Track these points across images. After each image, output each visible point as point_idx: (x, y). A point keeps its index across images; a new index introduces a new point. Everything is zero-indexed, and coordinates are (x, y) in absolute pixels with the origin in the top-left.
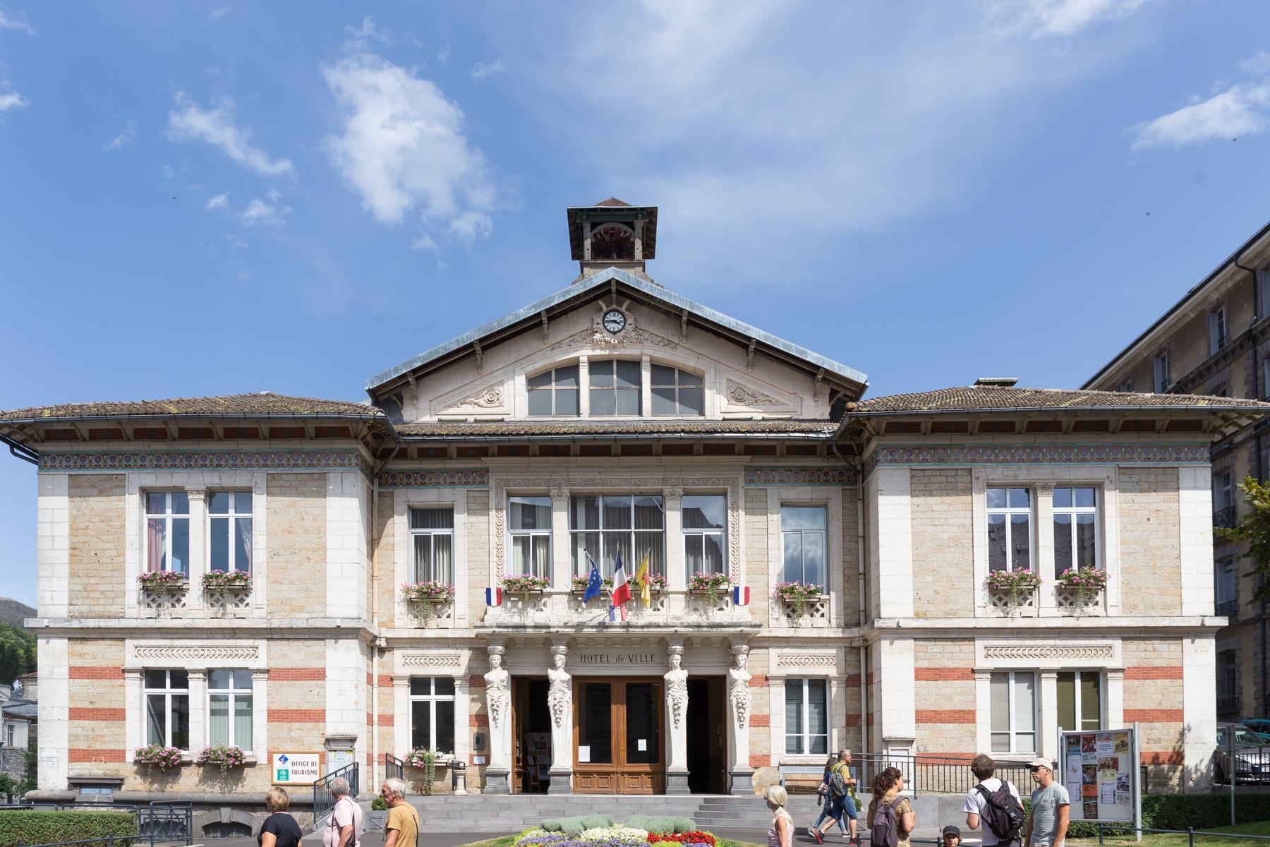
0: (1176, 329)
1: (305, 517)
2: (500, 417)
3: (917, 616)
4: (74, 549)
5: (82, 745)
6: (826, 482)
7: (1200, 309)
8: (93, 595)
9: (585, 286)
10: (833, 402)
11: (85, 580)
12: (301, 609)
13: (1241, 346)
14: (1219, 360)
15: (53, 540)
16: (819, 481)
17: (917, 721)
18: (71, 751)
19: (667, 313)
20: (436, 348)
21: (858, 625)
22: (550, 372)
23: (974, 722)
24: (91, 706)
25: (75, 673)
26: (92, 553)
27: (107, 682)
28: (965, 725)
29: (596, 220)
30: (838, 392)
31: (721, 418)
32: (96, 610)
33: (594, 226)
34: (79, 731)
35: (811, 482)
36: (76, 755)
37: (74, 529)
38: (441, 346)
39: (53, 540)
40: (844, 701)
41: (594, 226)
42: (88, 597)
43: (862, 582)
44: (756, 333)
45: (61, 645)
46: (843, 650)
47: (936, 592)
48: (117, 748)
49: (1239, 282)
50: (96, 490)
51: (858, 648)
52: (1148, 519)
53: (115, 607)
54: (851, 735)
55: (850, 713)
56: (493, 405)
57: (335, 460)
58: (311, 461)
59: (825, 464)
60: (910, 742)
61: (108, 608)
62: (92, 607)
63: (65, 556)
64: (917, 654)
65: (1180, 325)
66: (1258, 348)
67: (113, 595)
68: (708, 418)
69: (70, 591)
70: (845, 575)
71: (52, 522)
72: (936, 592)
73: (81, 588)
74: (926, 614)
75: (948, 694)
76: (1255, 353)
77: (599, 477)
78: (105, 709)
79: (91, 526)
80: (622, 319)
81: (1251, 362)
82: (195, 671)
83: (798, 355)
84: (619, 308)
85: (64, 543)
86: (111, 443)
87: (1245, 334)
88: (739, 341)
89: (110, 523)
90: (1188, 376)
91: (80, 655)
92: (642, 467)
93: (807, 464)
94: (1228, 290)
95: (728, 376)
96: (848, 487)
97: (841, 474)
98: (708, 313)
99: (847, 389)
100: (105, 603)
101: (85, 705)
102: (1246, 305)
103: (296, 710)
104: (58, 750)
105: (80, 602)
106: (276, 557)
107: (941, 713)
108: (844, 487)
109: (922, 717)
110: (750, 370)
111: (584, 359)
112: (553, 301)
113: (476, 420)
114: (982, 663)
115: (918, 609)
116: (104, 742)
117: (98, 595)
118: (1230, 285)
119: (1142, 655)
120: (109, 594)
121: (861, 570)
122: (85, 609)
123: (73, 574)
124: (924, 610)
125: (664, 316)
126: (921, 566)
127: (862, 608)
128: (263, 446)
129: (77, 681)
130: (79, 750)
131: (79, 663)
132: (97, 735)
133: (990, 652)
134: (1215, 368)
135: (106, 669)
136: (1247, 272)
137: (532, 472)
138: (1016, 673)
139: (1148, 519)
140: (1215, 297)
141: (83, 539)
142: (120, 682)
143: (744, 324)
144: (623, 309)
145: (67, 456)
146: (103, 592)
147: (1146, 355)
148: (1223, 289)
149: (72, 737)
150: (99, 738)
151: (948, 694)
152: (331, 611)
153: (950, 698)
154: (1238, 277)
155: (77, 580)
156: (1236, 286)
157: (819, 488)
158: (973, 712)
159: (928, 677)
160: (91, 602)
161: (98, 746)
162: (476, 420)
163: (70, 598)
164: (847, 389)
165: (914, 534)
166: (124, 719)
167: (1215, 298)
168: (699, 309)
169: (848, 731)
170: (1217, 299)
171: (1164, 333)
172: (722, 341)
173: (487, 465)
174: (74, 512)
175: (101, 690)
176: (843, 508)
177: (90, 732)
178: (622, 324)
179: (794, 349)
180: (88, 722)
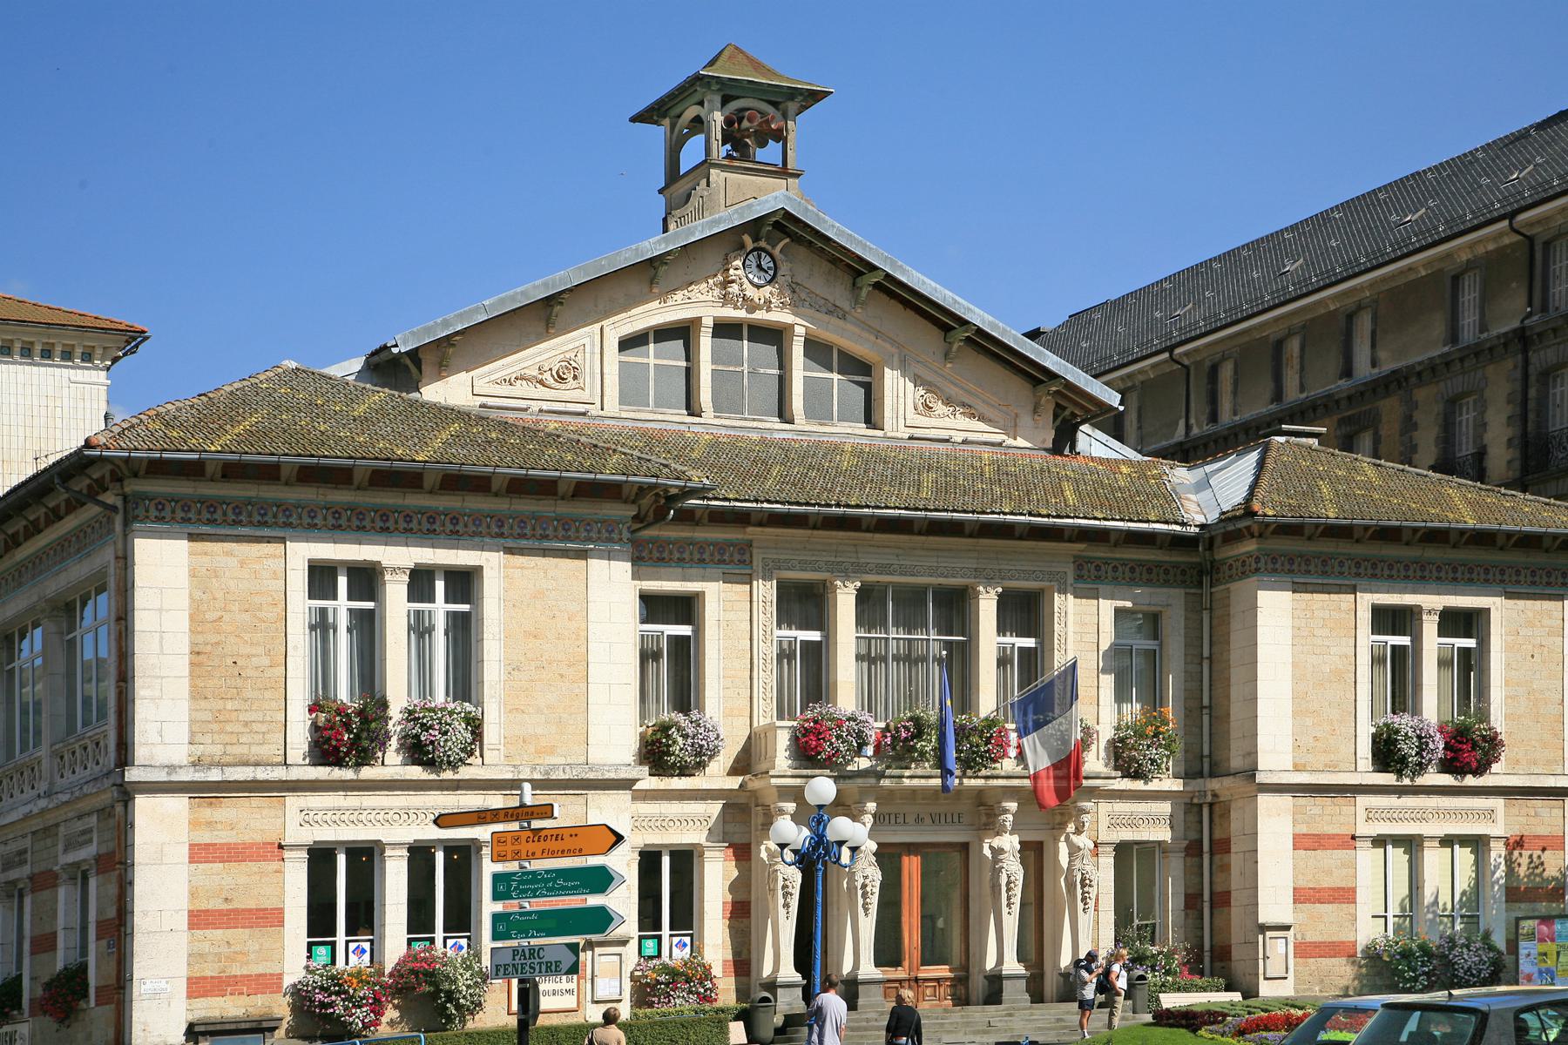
0: (1393, 284)
1: (558, 614)
2: (580, 408)
3: (1297, 768)
4: (198, 653)
5: (210, 970)
6: (1166, 583)
7: (1437, 266)
8: (229, 728)
9: (742, 217)
10: (1058, 422)
11: (220, 704)
12: (551, 750)
13: (1505, 345)
14: (1468, 355)
15: (162, 638)
16: (1158, 580)
17: (1295, 902)
18: (191, 981)
19: (834, 261)
20: (511, 292)
21: (1200, 775)
22: (647, 334)
23: (1354, 902)
24: (225, 906)
25: (200, 853)
26: (229, 661)
27: (253, 866)
28: (1344, 906)
29: (729, 92)
30: (1065, 408)
31: (907, 436)
32: (234, 752)
33: (726, 100)
34: (206, 947)
35: (1149, 583)
36: (198, 987)
37: (196, 620)
38: (519, 290)
39: (162, 638)
40: (1182, 875)
41: (726, 100)
42: (221, 732)
43: (1206, 719)
44: (979, 317)
45: (178, 804)
46: (1183, 806)
47: (1316, 739)
48: (268, 971)
49: (1506, 246)
50: (235, 559)
51: (1201, 806)
52: (1533, 656)
53: (266, 747)
54: (1190, 921)
55: (1190, 891)
56: (563, 386)
57: (599, 532)
58: (544, 529)
59: (1167, 558)
60: (1287, 928)
61: (255, 749)
62: (228, 747)
63: (182, 665)
64: (1296, 816)
65: (1402, 281)
66: (1530, 354)
67: (264, 728)
68: (889, 434)
69: (192, 722)
70: (1186, 708)
71: (160, 610)
72: (1316, 739)
73: (208, 716)
74: (1305, 766)
75: (1327, 867)
76: (1526, 362)
77: (897, 562)
78: (250, 910)
79: (227, 617)
80: (771, 265)
81: (1518, 374)
82: (394, 845)
83: (1032, 357)
84: (769, 248)
85: (181, 644)
86: (264, 488)
87: (1514, 331)
88: (943, 321)
89: (260, 614)
90: (1413, 366)
91: (209, 824)
92: (950, 550)
93: (1147, 557)
94: (1487, 252)
95: (916, 371)
96: (1193, 591)
97: (1183, 572)
98: (916, 281)
99: (1076, 404)
100: (251, 740)
101: (217, 904)
102: (1514, 285)
103: (257, 910)
104: (169, 979)
105: (208, 739)
106: (516, 673)
107: (1319, 890)
108: (1188, 590)
109: (1301, 896)
110: (949, 365)
111: (708, 322)
112: (693, 234)
113: (541, 411)
114: (1364, 829)
115: (1297, 760)
116: (247, 963)
117: (238, 728)
118: (1491, 247)
119: (1523, 820)
120: (255, 727)
121: (1206, 702)
122: (217, 750)
123: (197, 694)
124: (1303, 761)
125: (829, 264)
126: (1301, 709)
127: (1206, 751)
128: (502, 505)
129: (201, 866)
130: (205, 978)
131: (206, 837)
132: (235, 953)
133: (1371, 815)
134: (1459, 365)
135: (252, 845)
136: (1519, 238)
137: (810, 550)
138: (1393, 841)
139: (1533, 656)
140: (1464, 257)
141: (213, 638)
142: (275, 865)
143: (933, 284)
144: (777, 252)
145: (185, 504)
146: (246, 724)
147: (1332, 308)
148: (1481, 250)
149: (194, 957)
150: (239, 957)
151: (1327, 867)
152: (595, 756)
153: (1329, 873)
154: (1506, 241)
155: (203, 704)
156: (1501, 251)
157: (1158, 590)
158: (1353, 890)
159: (1307, 846)
160: (227, 739)
161: (236, 970)
162: (541, 411)
163: (192, 733)
164: (1076, 404)
165: (1294, 665)
166: (281, 923)
167: (1464, 258)
168: (904, 272)
169: (1187, 915)
170: (1468, 260)
171: (1371, 285)
172: (910, 313)
173: (750, 537)
174: (198, 594)
175: (243, 880)
176: (1186, 619)
177: (224, 950)
178: (771, 272)
179: (916, 281)
180: (220, 932)
